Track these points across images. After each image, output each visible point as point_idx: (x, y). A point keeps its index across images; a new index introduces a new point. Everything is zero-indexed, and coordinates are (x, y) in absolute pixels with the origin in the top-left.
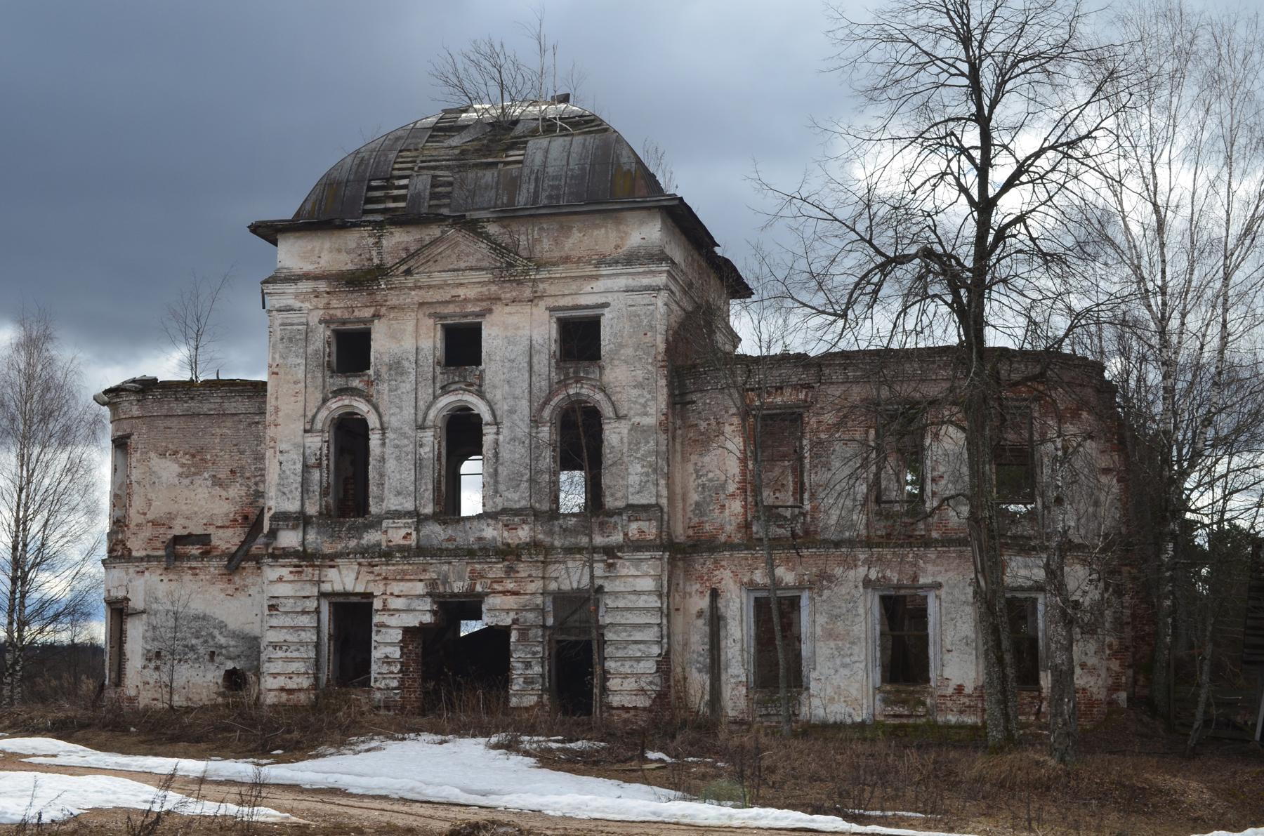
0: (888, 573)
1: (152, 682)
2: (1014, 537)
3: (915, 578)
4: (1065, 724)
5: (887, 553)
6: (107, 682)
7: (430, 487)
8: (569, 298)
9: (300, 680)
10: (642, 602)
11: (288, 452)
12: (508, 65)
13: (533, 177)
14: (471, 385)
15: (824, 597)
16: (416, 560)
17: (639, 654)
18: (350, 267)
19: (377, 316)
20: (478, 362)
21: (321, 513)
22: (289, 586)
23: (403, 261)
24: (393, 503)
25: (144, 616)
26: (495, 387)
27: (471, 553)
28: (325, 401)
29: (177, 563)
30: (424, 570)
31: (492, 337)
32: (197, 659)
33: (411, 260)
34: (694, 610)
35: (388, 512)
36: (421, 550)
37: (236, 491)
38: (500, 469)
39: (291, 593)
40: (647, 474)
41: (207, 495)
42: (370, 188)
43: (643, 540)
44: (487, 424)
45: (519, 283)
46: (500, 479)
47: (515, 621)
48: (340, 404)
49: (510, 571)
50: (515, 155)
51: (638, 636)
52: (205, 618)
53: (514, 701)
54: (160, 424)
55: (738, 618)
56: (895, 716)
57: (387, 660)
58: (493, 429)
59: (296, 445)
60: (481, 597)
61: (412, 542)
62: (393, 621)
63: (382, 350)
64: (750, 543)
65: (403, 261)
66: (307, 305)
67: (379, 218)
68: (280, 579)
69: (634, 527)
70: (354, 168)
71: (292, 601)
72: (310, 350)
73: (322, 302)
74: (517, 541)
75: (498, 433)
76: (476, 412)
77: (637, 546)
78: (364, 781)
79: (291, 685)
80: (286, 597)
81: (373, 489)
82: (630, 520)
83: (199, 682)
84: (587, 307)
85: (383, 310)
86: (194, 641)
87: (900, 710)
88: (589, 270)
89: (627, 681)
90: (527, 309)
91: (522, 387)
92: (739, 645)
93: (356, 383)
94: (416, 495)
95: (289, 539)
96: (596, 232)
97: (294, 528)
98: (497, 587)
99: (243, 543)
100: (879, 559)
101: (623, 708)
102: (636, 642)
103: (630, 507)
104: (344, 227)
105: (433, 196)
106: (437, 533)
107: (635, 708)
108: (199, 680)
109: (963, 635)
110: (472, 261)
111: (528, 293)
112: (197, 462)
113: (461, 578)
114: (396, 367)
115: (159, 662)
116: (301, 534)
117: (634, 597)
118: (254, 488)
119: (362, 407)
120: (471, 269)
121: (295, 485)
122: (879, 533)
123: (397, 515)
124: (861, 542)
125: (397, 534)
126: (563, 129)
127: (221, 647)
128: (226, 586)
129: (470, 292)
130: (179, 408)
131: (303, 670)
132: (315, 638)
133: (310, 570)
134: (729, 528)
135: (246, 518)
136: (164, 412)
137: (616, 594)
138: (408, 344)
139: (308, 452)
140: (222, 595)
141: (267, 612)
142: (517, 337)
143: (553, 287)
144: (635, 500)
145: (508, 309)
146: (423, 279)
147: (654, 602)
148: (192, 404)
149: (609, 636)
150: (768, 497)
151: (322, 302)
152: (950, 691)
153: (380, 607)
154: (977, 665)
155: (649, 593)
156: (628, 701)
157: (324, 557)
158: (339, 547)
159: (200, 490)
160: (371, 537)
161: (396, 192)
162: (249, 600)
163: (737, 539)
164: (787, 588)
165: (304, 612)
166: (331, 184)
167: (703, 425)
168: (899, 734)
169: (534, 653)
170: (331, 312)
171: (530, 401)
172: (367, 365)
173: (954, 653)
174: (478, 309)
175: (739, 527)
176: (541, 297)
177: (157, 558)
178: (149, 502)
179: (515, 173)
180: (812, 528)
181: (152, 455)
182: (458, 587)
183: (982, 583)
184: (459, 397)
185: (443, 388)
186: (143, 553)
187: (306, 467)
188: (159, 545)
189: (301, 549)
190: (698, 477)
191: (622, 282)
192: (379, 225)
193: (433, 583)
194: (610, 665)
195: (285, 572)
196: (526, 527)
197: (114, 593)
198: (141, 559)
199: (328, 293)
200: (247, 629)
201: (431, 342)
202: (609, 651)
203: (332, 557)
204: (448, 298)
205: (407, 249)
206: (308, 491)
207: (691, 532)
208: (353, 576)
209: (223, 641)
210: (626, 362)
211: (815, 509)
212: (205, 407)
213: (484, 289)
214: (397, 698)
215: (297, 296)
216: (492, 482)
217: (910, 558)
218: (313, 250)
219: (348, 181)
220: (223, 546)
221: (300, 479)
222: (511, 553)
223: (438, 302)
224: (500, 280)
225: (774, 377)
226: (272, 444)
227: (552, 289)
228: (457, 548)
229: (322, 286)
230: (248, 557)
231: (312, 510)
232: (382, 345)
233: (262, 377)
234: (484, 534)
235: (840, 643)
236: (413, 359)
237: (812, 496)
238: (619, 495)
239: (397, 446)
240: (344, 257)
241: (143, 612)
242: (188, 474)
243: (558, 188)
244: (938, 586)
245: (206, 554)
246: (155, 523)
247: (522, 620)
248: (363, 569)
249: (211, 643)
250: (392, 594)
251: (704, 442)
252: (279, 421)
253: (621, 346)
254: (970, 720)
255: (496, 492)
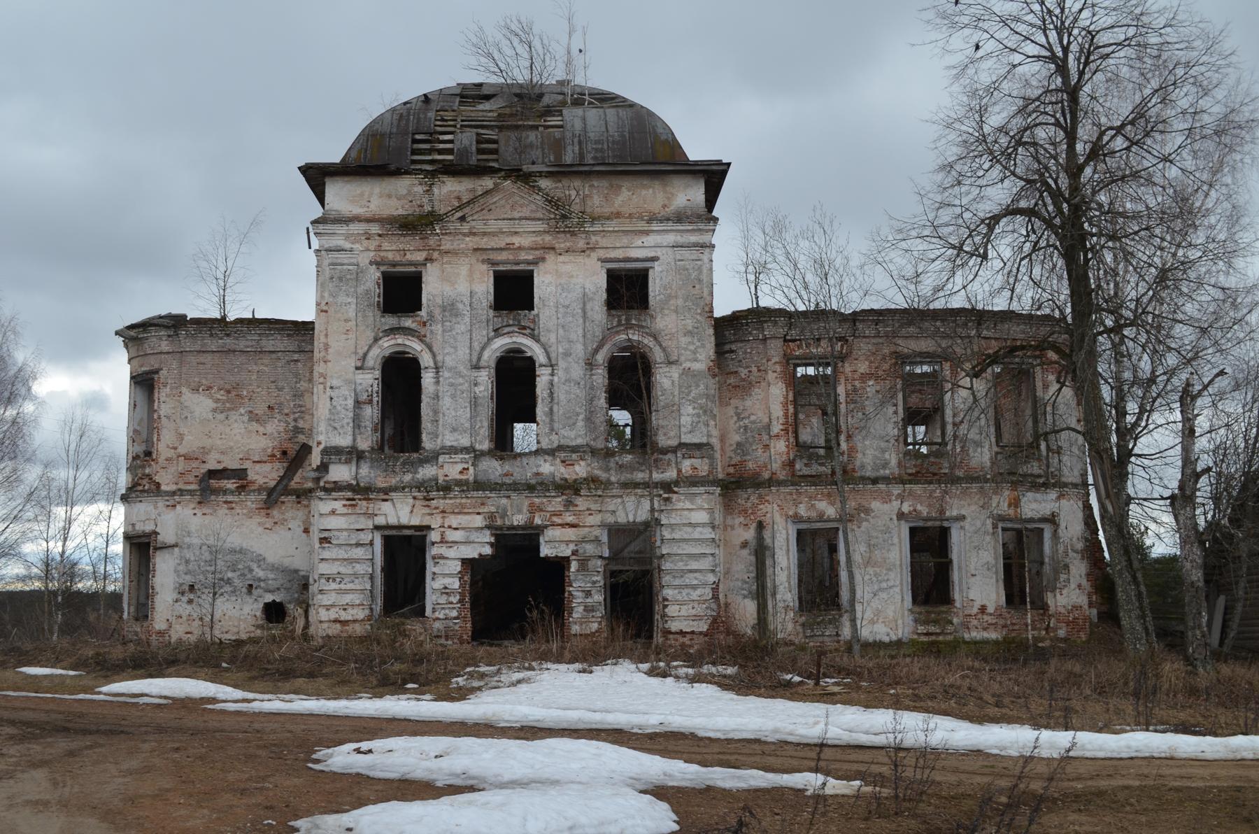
0: (919, 507)
1: (185, 615)
2: (1025, 476)
3: (942, 512)
4: (1203, 636)
5: (918, 488)
6: (125, 616)
7: (486, 424)
8: (620, 251)
9: (355, 611)
10: (697, 533)
11: (339, 388)
12: (536, 43)
13: (576, 140)
14: (524, 328)
15: (863, 529)
16: (475, 494)
17: (695, 582)
18: (400, 212)
19: (429, 260)
20: (530, 307)
21: (372, 448)
22: (343, 519)
23: (460, 208)
24: (449, 439)
25: (176, 549)
26: (549, 331)
27: (530, 488)
28: (376, 340)
29: (213, 497)
30: (483, 504)
31: (544, 285)
32: (234, 592)
33: (463, 207)
34: (738, 542)
35: (443, 448)
36: (479, 485)
37: (275, 427)
38: (555, 408)
39: (345, 526)
40: (698, 415)
41: (243, 431)
42: (415, 141)
43: (696, 476)
44: (541, 366)
45: (573, 234)
46: (556, 418)
47: (574, 553)
48: (392, 342)
49: (569, 504)
50: (554, 121)
51: (694, 565)
52: (241, 551)
53: (575, 629)
54: (193, 359)
55: (784, 548)
56: (927, 634)
57: (446, 591)
58: (549, 370)
59: (348, 382)
60: (540, 529)
61: (470, 475)
62: (451, 553)
63: (434, 292)
64: (796, 480)
65: (460, 208)
66: (356, 246)
67: (429, 167)
68: (333, 512)
69: (686, 465)
70: (395, 123)
71: (345, 533)
72: (361, 289)
73: (373, 244)
74: (574, 477)
75: (552, 375)
76: (529, 354)
77: (694, 481)
78: (597, 717)
79: (344, 616)
80: (338, 530)
81: (426, 424)
82: (684, 457)
83: (238, 616)
84: (637, 260)
85: (436, 255)
86: (230, 575)
87: (932, 629)
88: (642, 225)
89: (682, 608)
90: (580, 259)
91: (577, 333)
92: (786, 573)
93: (408, 322)
94: (473, 432)
95: (340, 473)
96: (644, 192)
97: (348, 462)
98: (556, 520)
99: (282, 478)
100: (910, 494)
101: (682, 633)
102: (691, 571)
103: (682, 445)
104: (398, 173)
105: (480, 151)
106: (493, 468)
107: (693, 632)
108: (235, 613)
109: (985, 561)
110: (526, 212)
111: (581, 244)
112: (232, 397)
113: (520, 512)
114: (450, 309)
115: (192, 596)
116: (354, 468)
117: (689, 529)
118: (293, 424)
119: (415, 346)
120: (526, 219)
121: (346, 421)
122: (910, 471)
123: (453, 450)
124: (894, 478)
125: (452, 469)
126: (590, 103)
127: (260, 580)
128: (264, 519)
129: (525, 241)
130: (213, 345)
131: (358, 602)
132: (370, 570)
133: (364, 503)
134: (776, 466)
135: (284, 453)
136: (198, 348)
137: (672, 527)
138: (462, 287)
139: (359, 388)
140: (260, 529)
141: (317, 545)
142: (569, 286)
143: (605, 240)
144: (686, 439)
145: (561, 258)
146: (479, 226)
147: (708, 533)
148: (228, 341)
149: (667, 566)
150: (805, 436)
151: (373, 244)
152: (975, 610)
153: (438, 540)
154: (997, 588)
155: (704, 525)
156: (686, 626)
157: (380, 490)
158: (394, 481)
159: (236, 425)
160: (427, 472)
161: (442, 146)
162: (289, 534)
163: (782, 475)
164: (829, 520)
165: (358, 545)
166: (373, 135)
167: (743, 372)
168: (932, 649)
169: (594, 583)
170: (382, 254)
171: (584, 345)
172: (418, 307)
173: (978, 578)
174: (531, 257)
175: (784, 465)
176: (593, 249)
177: (191, 492)
178: (181, 437)
179: (557, 135)
180: (850, 467)
181: (184, 390)
182: (519, 519)
183: (1110, 508)
184: (514, 339)
185: (496, 331)
186: (174, 488)
187: (358, 403)
188: (192, 479)
189: (354, 483)
190: (739, 419)
191: (671, 238)
192: (433, 174)
193: (491, 516)
194: (668, 593)
195: (338, 505)
196: (582, 463)
197: (140, 528)
198: (173, 493)
199: (380, 235)
200: (287, 562)
201: (485, 287)
202: (666, 579)
203: (386, 491)
204: (503, 245)
205: (459, 198)
206: (359, 427)
207: (731, 470)
208: (408, 509)
209: (261, 574)
210: (676, 311)
211: (852, 450)
212: (242, 344)
213: (539, 239)
214: (457, 627)
215: (347, 237)
216: (548, 420)
217: (938, 493)
218: (362, 195)
219: (391, 133)
220: (261, 481)
221: (351, 415)
222: (569, 487)
223: (492, 249)
224: (556, 231)
225: (818, 328)
226: (321, 380)
227: (603, 242)
228: (515, 483)
229: (375, 229)
230: (287, 492)
231: (364, 444)
232: (433, 287)
233: (306, 313)
234: (541, 470)
235: (878, 570)
236: (467, 303)
237: (849, 437)
238: (672, 434)
239: (452, 385)
240: (394, 202)
241: (176, 545)
242: (223, 409)
243: (602, 150)
244: (963, 518)
245: (242, 488)
246: (187, 458)
247: (581, 551)
248: (418, 503)
249: (249, 576)
250: (450, 527)
251: (744, 388)
252: (329, 357)
253: (670, 297)
254: (993, 635)
255: (552, 430)
